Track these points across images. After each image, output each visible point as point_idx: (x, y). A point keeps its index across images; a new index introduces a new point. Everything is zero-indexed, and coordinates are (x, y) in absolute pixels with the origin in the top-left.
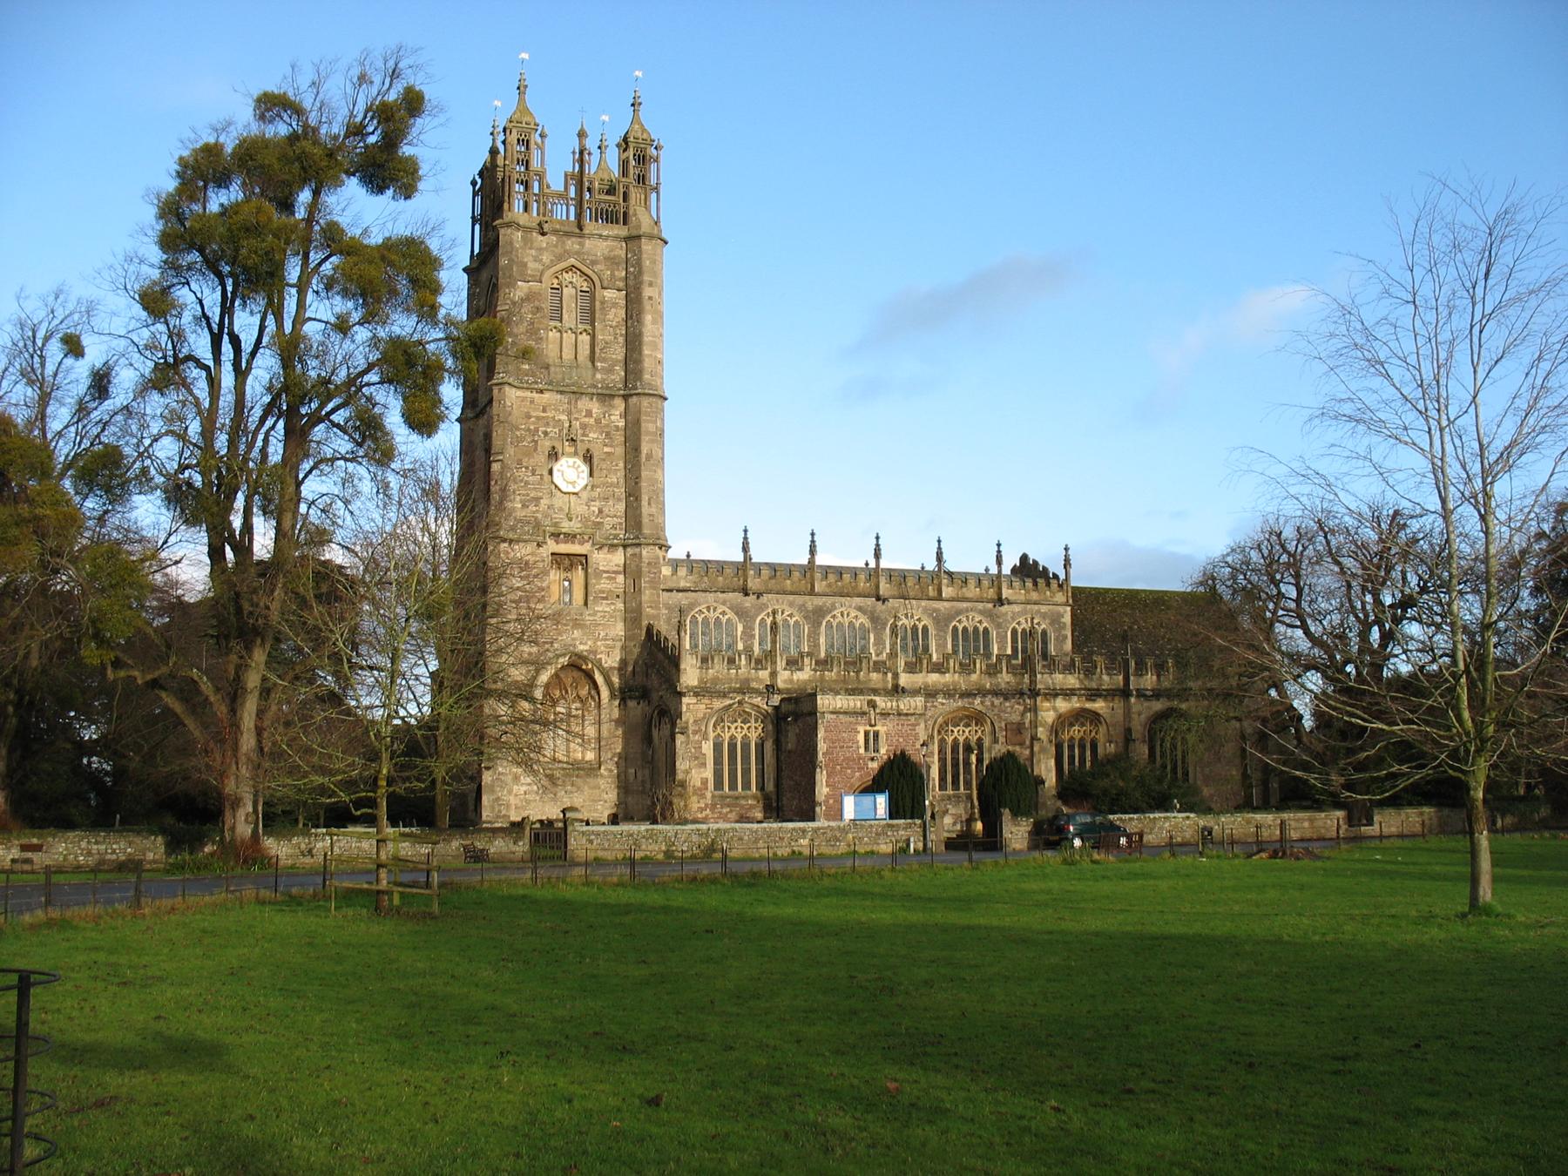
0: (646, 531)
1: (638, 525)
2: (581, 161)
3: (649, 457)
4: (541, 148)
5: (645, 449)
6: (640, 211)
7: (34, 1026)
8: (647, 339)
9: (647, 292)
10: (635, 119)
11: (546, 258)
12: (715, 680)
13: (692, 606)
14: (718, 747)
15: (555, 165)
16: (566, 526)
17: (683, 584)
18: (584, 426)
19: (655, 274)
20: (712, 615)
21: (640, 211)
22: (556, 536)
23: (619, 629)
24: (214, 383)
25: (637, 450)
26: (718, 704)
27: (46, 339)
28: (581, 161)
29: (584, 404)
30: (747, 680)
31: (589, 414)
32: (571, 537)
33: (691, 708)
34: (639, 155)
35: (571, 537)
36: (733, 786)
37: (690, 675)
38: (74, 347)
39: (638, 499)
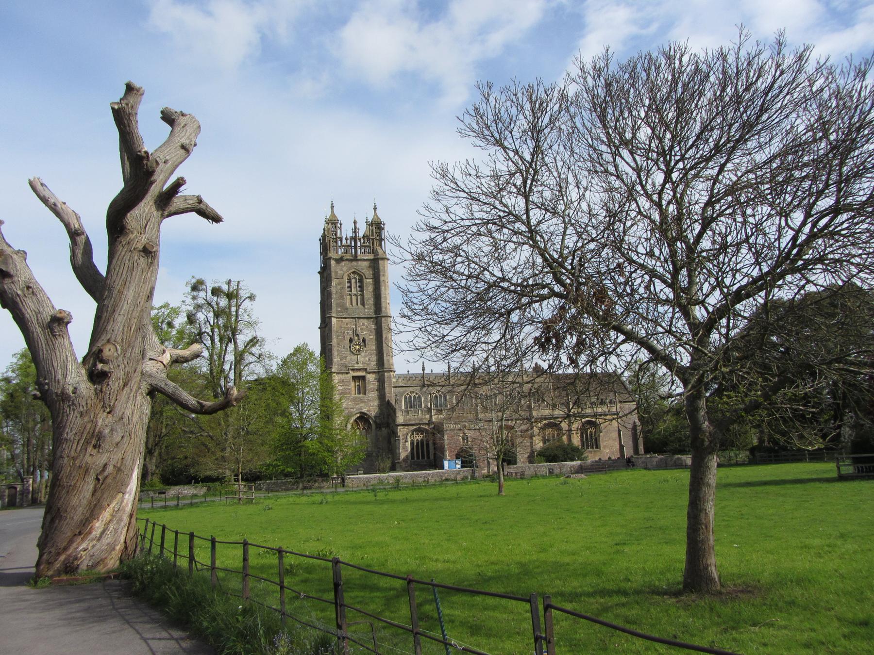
0: (386, 366)
1: (383, 364)
2: (355, 232)
3: (386, 338)
4: (340, 228)
5: (384, 337)
6: (379, 248)
7: (218, 564)
8: (383, 296)
9: (382, 278)
10: (375, 214)
11: (344, 269)
12: (410, 420)
13: (404, 392)
14: (412, 443)
15: (346, 232)
16: (356, 366)
17: (401, 384)
18: (362, 329)
19: (384, 272)
20: (412, 395)
21: (379, 248)
22: (353, 370)
23: (376, 403)
24: (213, 340)
25: (381, 336)
26: (411, 428)
27: (162, 323)
28: (355, 232)
29: (362, 321)
30: (422, 419)
31: (363, 324)
32: (359, 370)
33: (401, 431)
34: (377, 226)
35: (359, 370)
36: (418, 458)
37: (400, 419)
38: (170, 325)
39: (383, 354)
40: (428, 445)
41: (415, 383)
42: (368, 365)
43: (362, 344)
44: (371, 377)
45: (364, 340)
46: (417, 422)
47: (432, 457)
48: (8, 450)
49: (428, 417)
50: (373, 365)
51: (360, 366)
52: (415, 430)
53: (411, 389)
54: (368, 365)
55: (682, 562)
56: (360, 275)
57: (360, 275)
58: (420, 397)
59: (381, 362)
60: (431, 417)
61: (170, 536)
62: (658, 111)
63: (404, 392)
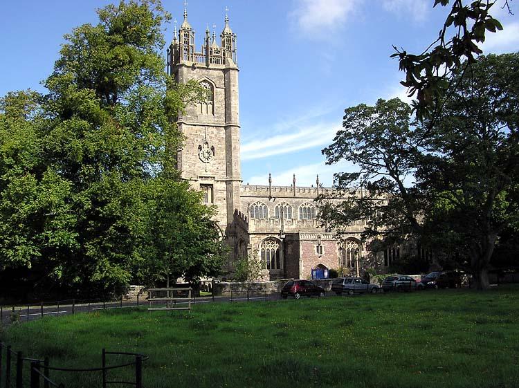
3: (235, 148)
12: (261, 229)
17: (248, 195)
18: (211, 137)
33: (254, 241)
39: (231, 164)
40: (268, 253)
41: (262, 193)
42: (216, 173)
43: (211, 152)
44: (218, 186)
45: (213, 149)
46: (269, 231)
47: (282, 267)
48: (418, 130)
49: (279, 227)
50: (221, 174)
51: (209, 174)
52: (267, 240)
53: (258, 199)
54: (216, 173)
55: (516, 334)
56: (211, 84)
57: (211, 84)
58: (265, 207)
59: (229, 170)
60: (282, 226)
61: (26, 364)
62: (97, 45)
63: (253, 201)
